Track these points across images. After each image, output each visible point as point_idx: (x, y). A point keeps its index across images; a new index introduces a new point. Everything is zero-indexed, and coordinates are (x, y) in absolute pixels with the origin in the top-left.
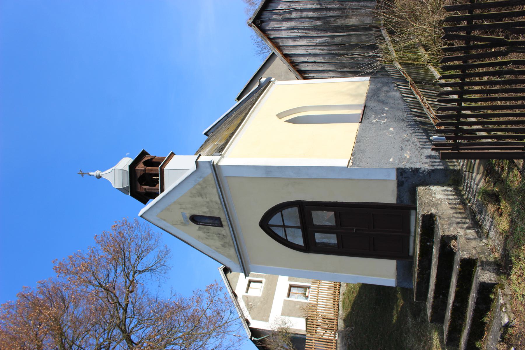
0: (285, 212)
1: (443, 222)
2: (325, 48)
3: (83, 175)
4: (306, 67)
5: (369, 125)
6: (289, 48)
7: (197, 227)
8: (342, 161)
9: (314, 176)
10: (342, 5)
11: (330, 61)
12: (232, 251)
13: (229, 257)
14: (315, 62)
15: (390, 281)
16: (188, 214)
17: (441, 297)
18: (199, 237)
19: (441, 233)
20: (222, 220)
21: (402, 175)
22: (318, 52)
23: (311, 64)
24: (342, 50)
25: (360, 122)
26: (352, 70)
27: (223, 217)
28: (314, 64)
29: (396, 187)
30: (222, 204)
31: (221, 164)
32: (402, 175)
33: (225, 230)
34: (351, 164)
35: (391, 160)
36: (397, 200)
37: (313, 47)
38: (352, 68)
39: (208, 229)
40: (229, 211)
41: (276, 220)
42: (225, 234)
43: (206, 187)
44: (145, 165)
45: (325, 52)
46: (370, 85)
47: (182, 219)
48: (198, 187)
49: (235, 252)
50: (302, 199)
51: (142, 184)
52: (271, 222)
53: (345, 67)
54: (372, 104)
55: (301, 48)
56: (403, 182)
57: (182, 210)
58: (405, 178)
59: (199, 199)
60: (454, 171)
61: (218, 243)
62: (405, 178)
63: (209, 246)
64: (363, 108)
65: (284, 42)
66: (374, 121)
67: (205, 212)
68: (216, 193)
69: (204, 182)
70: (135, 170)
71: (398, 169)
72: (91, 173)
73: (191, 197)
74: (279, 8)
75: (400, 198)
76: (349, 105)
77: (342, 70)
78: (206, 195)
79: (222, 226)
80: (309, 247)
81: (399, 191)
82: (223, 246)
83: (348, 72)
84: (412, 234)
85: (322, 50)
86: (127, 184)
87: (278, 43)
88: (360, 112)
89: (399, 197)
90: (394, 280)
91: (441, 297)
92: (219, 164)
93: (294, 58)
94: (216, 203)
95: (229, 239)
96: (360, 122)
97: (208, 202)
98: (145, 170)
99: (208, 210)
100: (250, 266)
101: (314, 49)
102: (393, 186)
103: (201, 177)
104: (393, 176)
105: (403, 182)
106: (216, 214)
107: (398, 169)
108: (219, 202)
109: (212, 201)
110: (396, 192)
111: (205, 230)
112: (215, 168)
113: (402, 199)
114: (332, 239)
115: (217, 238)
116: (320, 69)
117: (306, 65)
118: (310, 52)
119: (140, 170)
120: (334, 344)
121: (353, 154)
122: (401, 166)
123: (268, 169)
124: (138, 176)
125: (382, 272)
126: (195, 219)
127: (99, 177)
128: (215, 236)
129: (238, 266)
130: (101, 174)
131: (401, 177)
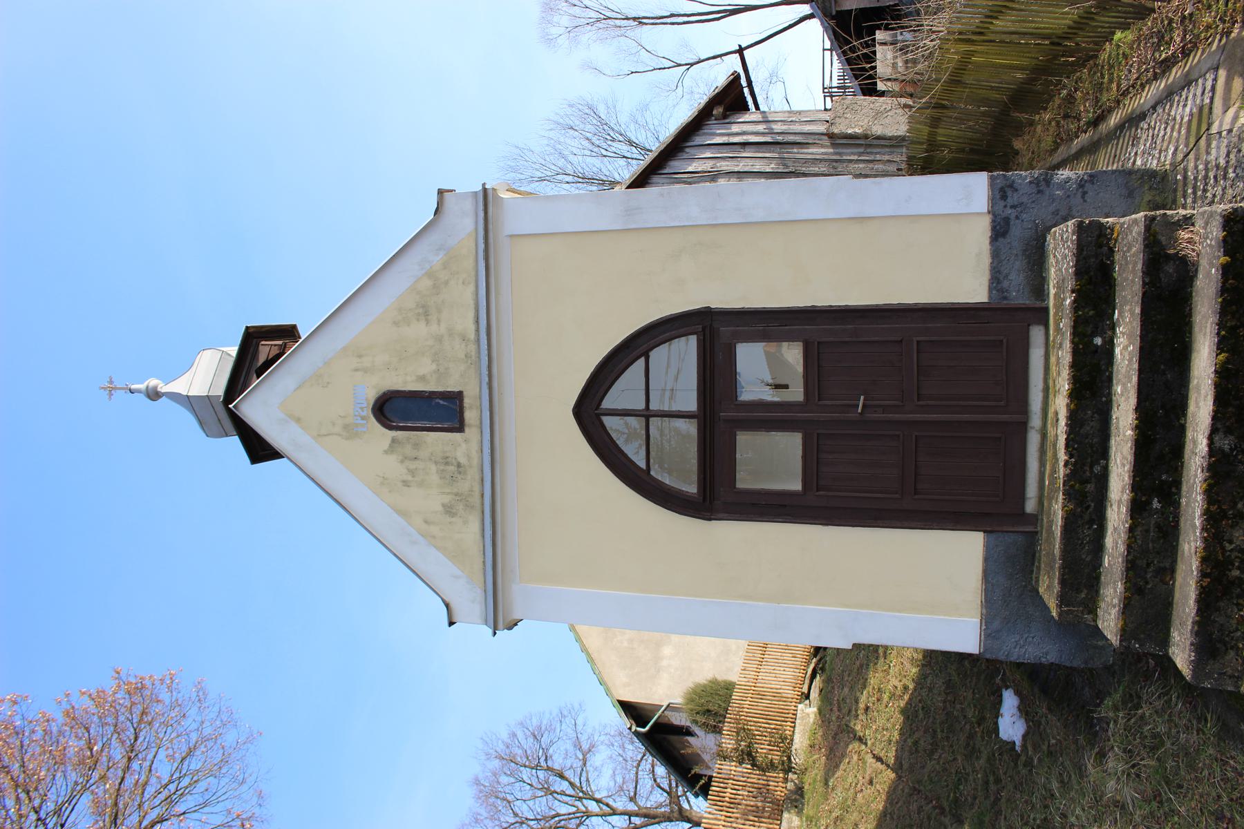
0: (659, 355)
3: (111, 390)
9: (759, 216)
10: (834, 168)
13: (457, 556)
17: (1156, 504)
20: (467, 401)
21: (1004, 197)
29: (987, 241)
30: (478, 341)
32: (1004, 197)
33: (463, 446)
39: (416, 446)
40: (494, 354)
41: (625, 392)
42: (463, 460)
43: (447, 283)
48: (428, 283)
49: (478, 537)
50: (715, 304)
52: (611, 401)
56: (1007, 220)
58: (1013, 207)
59: (419, 330)
60: (1151, 175)
62: (1013, 207)
63: (403, 513)
67: (422, 378)
68: (472, 303)
69: (445, 266)
73: (396, 324)
74: (690, 169)
75: (999, 282)
78: (439, 311)
80: (713, 495)
81: (995, 254)
82: (449, 510)
84: (1035, 422)
89: (990, 297)
90: (976, 621)
91: (1156, 504)
95: (469, 484)
97: (439, 339)
99: (434, 367)
105: (1007, 220)
108: (472, 336)
109: (451, 332)
110: (986, 260)
111: (408, 450)
113: (1005, 284)
115: (434, 478)
128: (433, 468)
129: (478, 594)
131: (1002, 203)
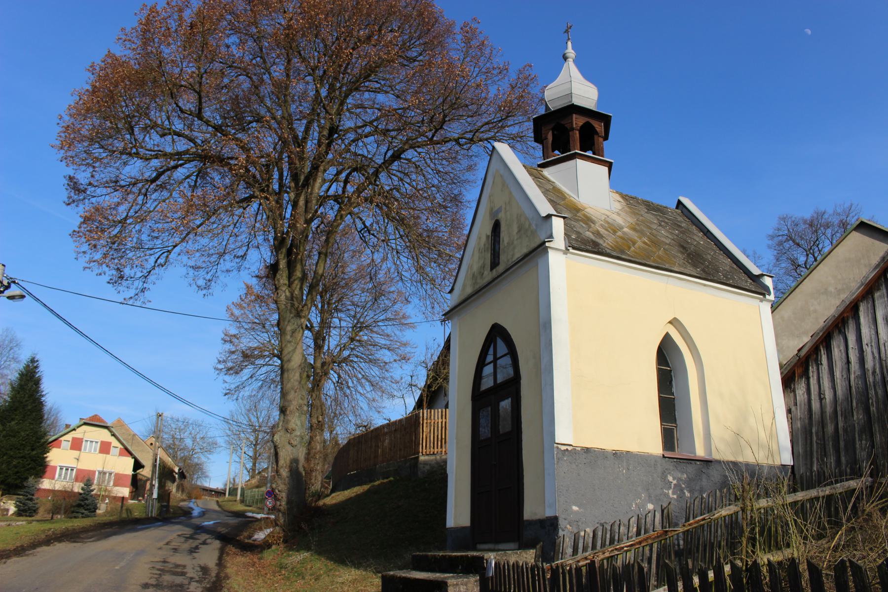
1: (470, 585)
2: (879, 377)
3: (567, 31)
4: (839, 347)
5: (660, 469)
6: (871, 311)
7: (489, 233)
8: (566, 433)
11: (854, 389)
12: (469, 290)
13: (464, 286)
14: (848, 362)
15: (450, 523)
16: (501, 216)
18: (480, 238)
19: (450, 582)
22: (869, 364)
23: (844, 355)
24: (877, 408)
25: (664, 456)
26: (841, 432)
27: (501, 268)
28: (845, 360)
31: (551, 254)
34: (563, 448)
35: (575, 508)
36: (527, 521)
37: (877, 355)
38: (845, 430)
44: (582, 127)
45: (871, 379)
46: (771, 467)
47: (496, 209)
51: (553, 130)
53: (846, 418)
54: (715, 474)
55: (873, 332)
57: (504, 207)
61: (475, 268)
64: (707, 458)
65: (881, 301)
66: (670, 478)
70: (571, 114)
71: (556, 519)
72: (569, 43)
76: (710, 434)
77: (839, 413)
79: (492, 269)
83: (837, 424)
85: (874, 372)
86: (552, 107)
87: (879, 289)
88: (700, 452)
89: (530, 523)
92: (549, 250)
93: (851, 325)
94: (513, 255)
96: (664, 456)
98: (573, 129)
100: (456, 319)
101: (874, 358)
102: (539, 516)
103: (536, 225)
104: (549, 513)
106: (503, 258)
107: (556, 519)
112: (540, 249)
114: (485, 432)
116: (838, 374)
117: (842, 348)
118: (868, 350)
119: (572, 123)
120: (436, 450)
121: (587, 450)
122: (562, 523)
123: (547, 326)
124: (562, 122)
125: (458, 512)
126: (496, 227)
127: (565, 58)
130: (570, 62)
